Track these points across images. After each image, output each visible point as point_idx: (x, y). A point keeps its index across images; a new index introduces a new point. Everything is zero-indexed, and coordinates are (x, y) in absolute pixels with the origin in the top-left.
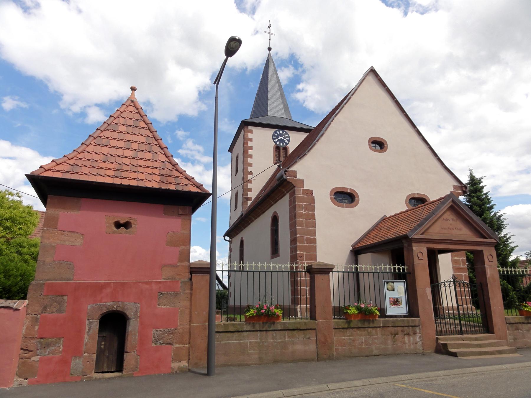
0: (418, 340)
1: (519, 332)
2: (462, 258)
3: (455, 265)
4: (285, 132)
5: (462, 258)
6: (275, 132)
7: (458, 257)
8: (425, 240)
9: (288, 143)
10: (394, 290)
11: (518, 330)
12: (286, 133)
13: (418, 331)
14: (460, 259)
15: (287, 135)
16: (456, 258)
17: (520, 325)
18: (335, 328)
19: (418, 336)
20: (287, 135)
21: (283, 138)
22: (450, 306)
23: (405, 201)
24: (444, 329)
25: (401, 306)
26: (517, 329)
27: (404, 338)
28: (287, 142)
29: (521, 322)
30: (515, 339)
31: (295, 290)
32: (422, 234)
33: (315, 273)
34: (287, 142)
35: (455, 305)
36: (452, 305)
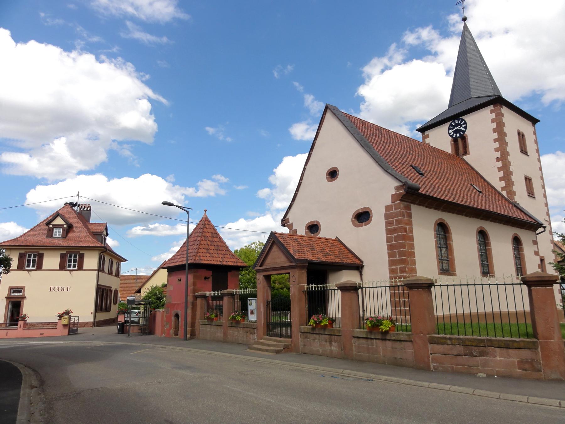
0: (256, 338)
1: (308, 340)
2: (399, 266)
3: (392, 274)
4: (461, 119)
5: (399, 266)
6: (451, 125)
7: (395, 266)
8: (271, 269)
9: (465, 131)
10: (252, 305)
11: (307, 338)
12: (463, 120)
13: (256, 332)
14: (397, 268)
15: (463, 122)
16: (394, 267)
17: (309, 334)
18: (228, 326)
19: (256, 334)
20: (463, 122)
21: (459, 127)
22: (502, 311)
23: (351, 219)
24: (288, 334)
25: (254, 315)
26: (306, 338)
27: (250, 335)
28: (464, 130)
29: (309, 332)
30: (304, 345)
31: (394, 293)
32: (260, 266)
33: (226, 294)
34: (464, 130)
35: (528, 309)
36: (508, 310)
